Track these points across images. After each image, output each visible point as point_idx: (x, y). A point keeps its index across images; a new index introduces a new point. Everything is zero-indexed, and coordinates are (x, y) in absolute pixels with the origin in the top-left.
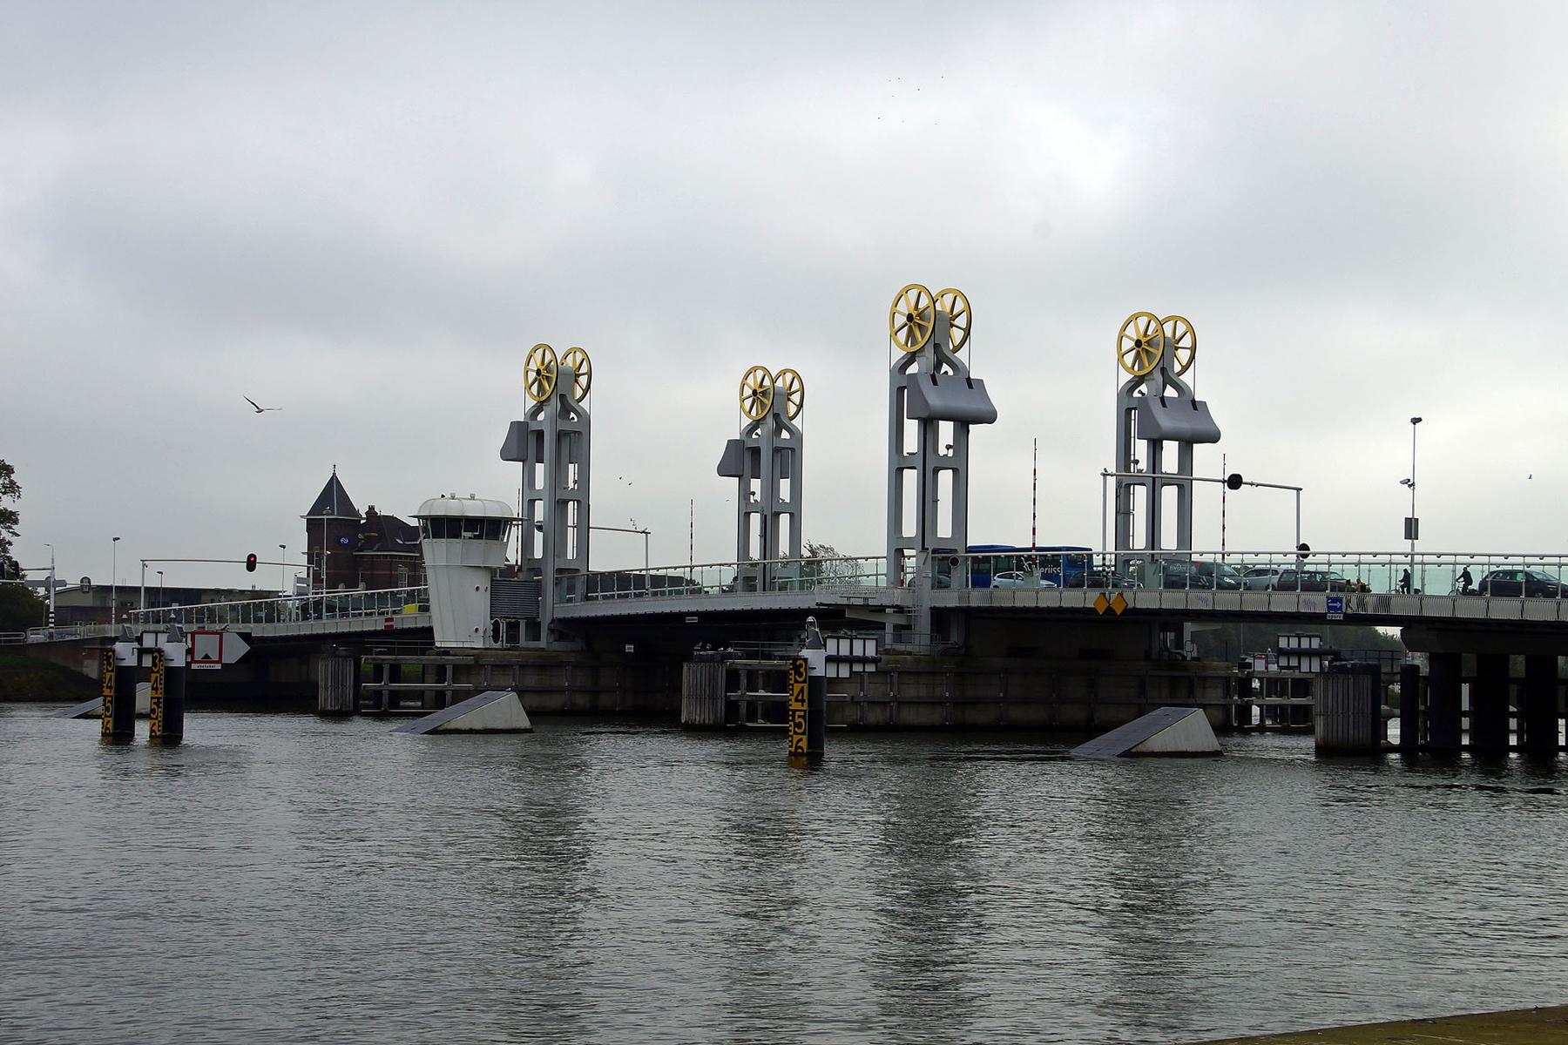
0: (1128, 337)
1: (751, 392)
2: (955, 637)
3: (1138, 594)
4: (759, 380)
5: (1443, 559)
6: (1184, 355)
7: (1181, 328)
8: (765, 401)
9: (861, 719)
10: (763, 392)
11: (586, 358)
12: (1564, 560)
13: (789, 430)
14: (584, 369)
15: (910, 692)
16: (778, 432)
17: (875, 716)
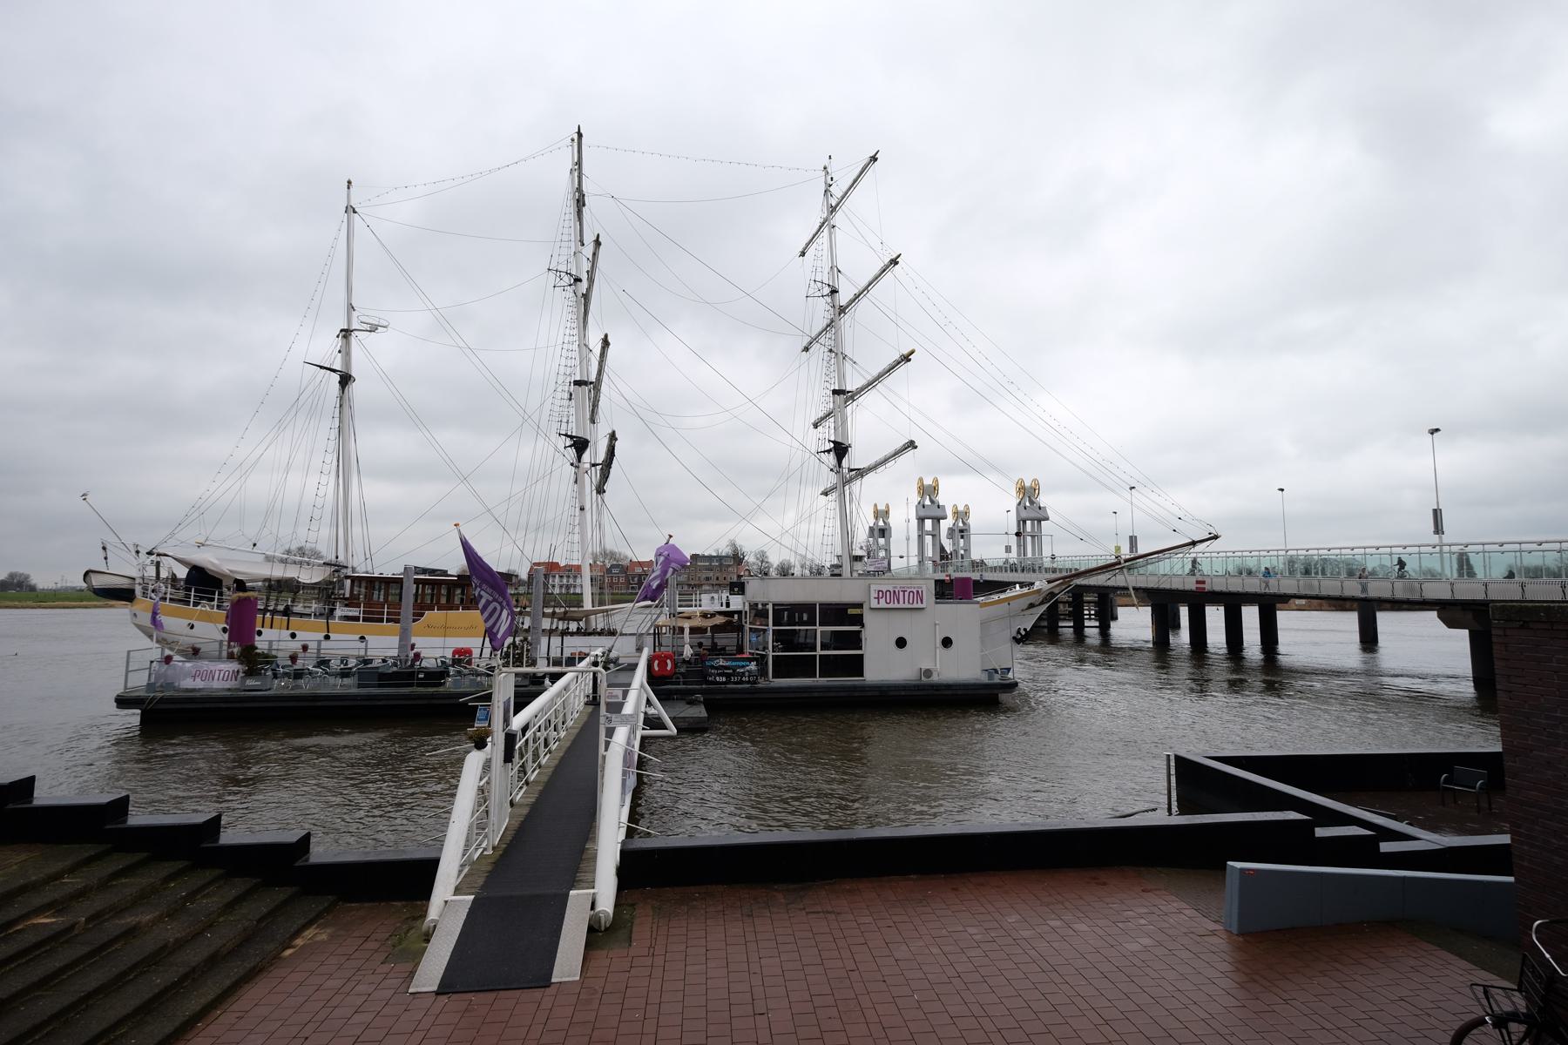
0: (853, 999)
3: (1281, 582)
5: (1506, 547)
12: (1564, 546)
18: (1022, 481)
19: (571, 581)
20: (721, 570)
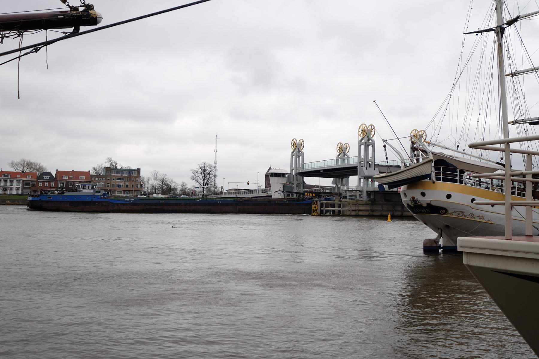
1: (361, 130)
2: (372, 197)
4: (364, 128)
6: (373, 133)
7: (373, 127)
8: (365, 133)
9: (350, 214)
10: (364, 131)
11: (303, 141)
13: (371, 140)
14: (303, 143)
15: (361, 208)
16: (368, 140)
17: (353, 213)
18: (296, 140)
19: (8, 184)
20: (130, 180)
